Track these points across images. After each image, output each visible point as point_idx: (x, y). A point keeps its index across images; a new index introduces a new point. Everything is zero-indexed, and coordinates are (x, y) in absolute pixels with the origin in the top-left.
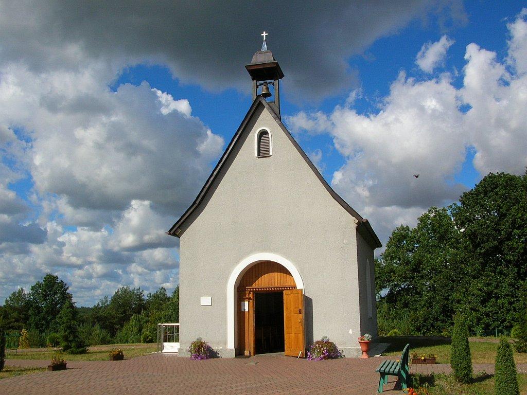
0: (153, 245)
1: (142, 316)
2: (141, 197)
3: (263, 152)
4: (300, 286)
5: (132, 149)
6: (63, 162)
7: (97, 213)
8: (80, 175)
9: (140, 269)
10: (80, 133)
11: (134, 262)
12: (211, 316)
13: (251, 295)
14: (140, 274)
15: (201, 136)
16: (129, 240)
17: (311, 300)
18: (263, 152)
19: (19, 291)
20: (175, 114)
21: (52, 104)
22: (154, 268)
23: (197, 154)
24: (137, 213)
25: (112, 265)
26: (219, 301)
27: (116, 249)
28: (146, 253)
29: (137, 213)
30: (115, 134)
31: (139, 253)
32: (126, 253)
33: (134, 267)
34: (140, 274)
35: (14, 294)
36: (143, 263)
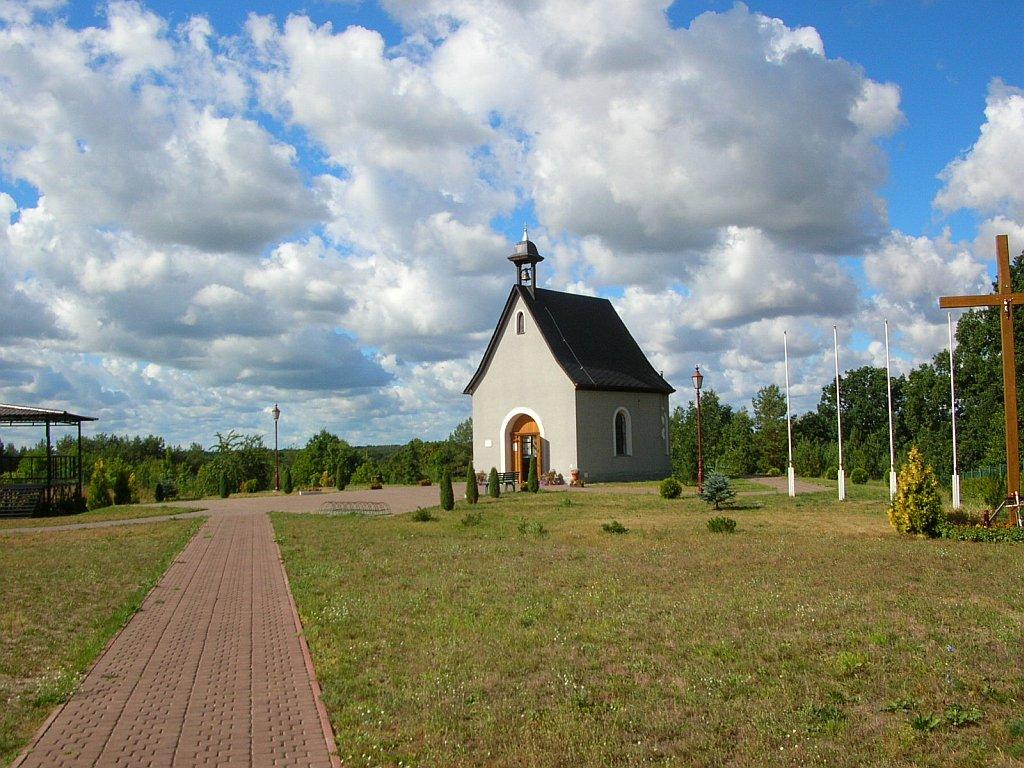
0: (771, 312)
1: (454, 457)
2: (741, 223)
3: (520, 330)
4: (542, 435)
5: (719, 134)
6: (591, 168)
7: (658, 259)
8: (621, 191)
9: (744, 361)
10: (619, 111)
11: (731, 348)
12: (491, 455)
13: (519, 439)
14: (744, 370)
15: (852, 91)
16: (722, 306)
17: (547, 443)
18: (520, 330)
19: (467, 423)
20: (800, 56)
21: (565, 64)
22: (772, 356)
23: (850, 128)
24: (739, 252)
25: (688, 354)
26: (496, 442)
27: (698, 324)
28: (755, 328)
29: (739, 252)
30: (686, 101)
31: (742, 329)
32: (718, 332)
33: (730, 357)
34: (744, 370)
35: (460, 427)
36: (750, 350)
